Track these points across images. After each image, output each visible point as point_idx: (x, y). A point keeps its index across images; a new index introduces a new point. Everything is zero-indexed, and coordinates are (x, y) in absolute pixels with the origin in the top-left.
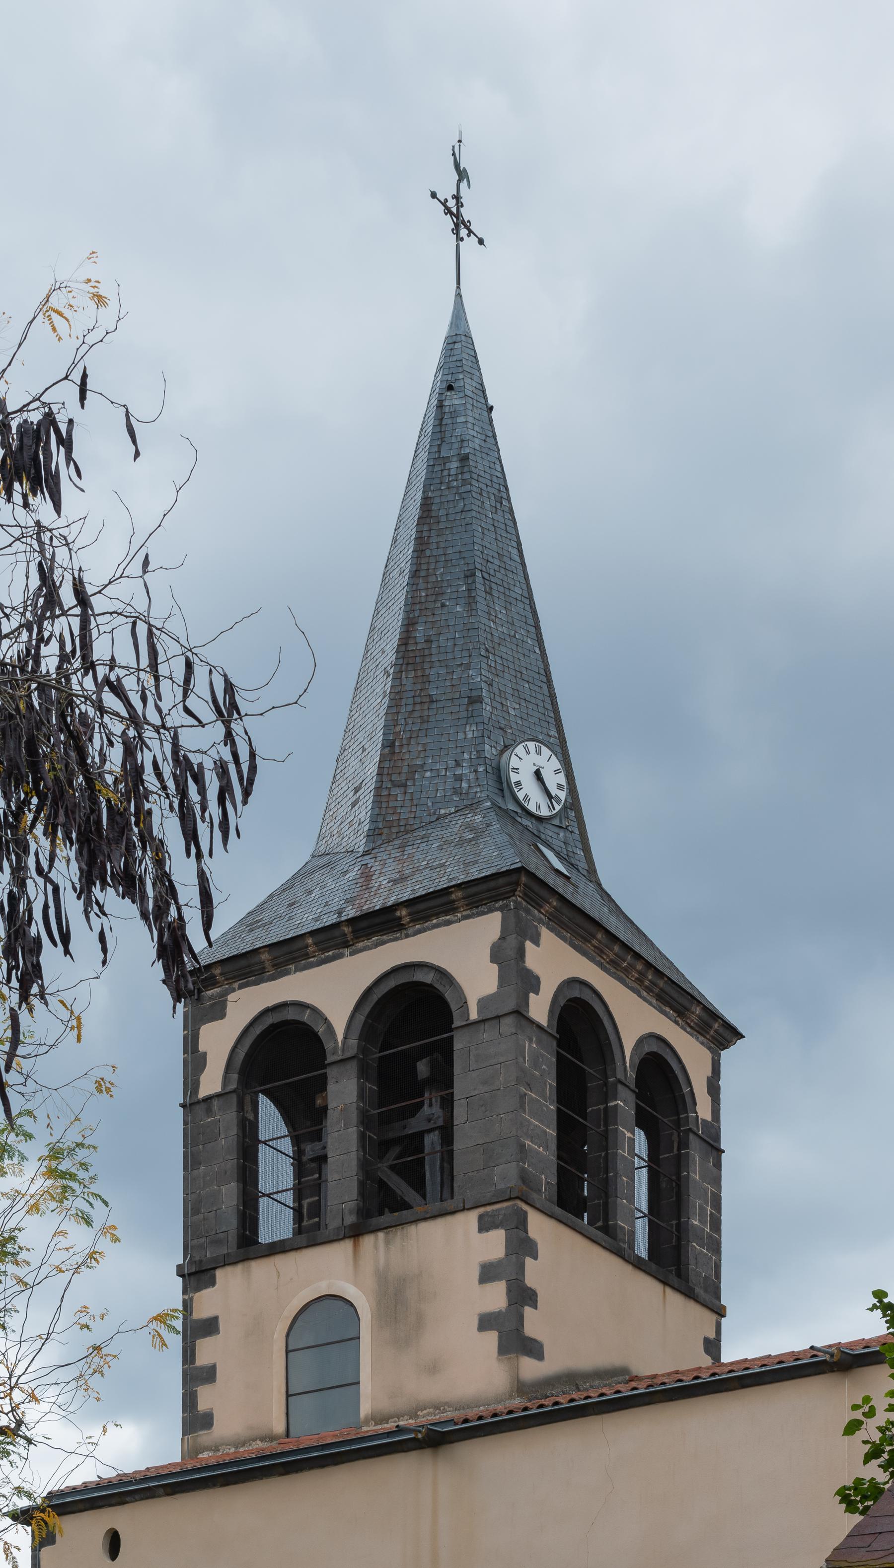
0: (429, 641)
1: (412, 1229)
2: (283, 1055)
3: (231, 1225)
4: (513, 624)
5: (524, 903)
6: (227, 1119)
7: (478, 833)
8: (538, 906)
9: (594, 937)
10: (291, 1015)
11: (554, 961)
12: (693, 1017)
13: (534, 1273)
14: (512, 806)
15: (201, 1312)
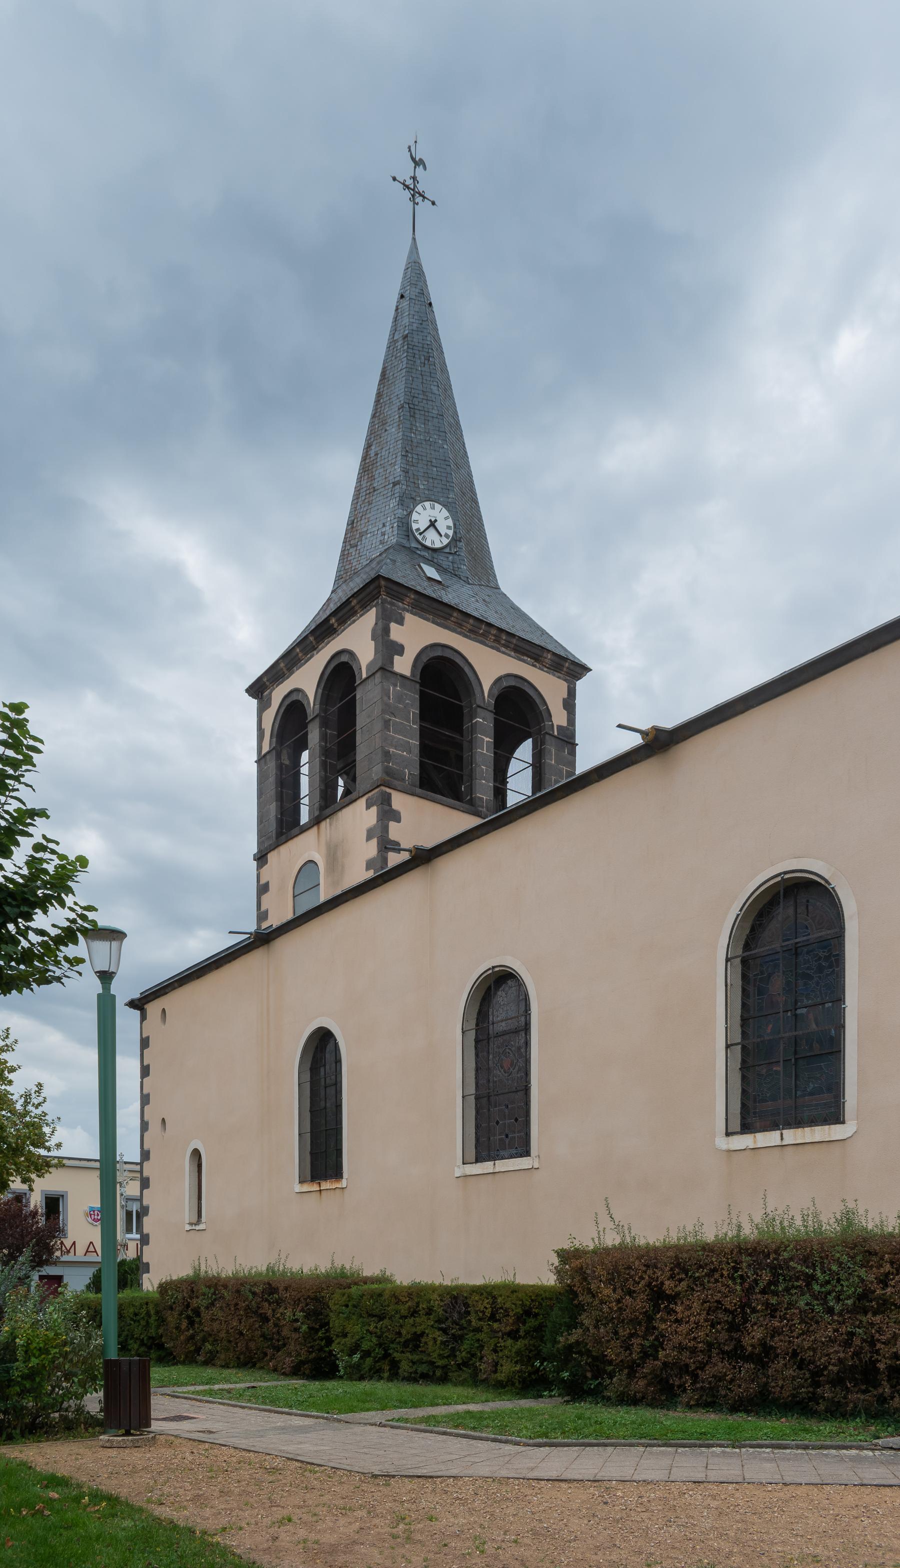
0: (377, 454)
1: (340, 814)
4: (428, 433)
5: (389, 599)
8: (402, 601)
9: (451, 616)
11: (416, 635)
12: (547, 661)
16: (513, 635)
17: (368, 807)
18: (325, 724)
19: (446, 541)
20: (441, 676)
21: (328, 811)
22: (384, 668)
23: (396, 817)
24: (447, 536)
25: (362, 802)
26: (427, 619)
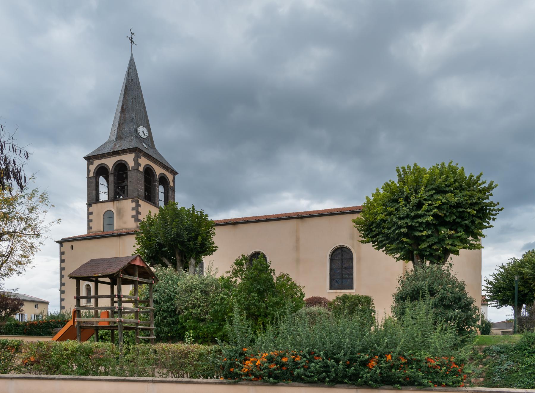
2: (102, 171)
3: (95, 197)
6: (94, 181)
7: (132, 140)
10: (103, 165)
11: (144, 162)
13: (140, 209)
15: (90, 211)
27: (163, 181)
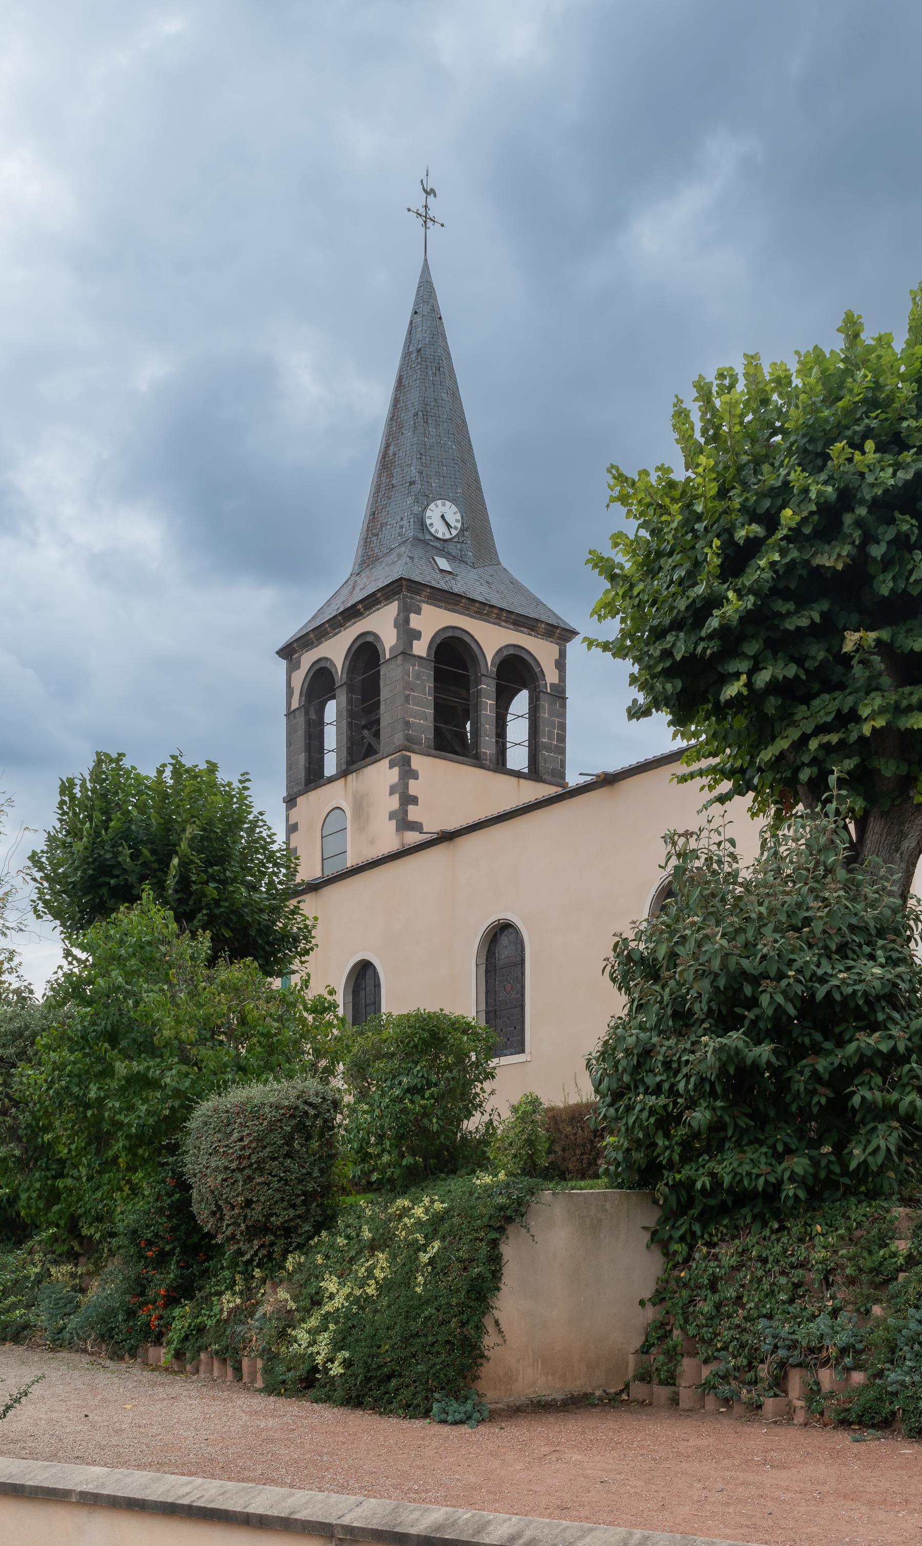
1: (365, 770)
8: (420, 595)
13: (414, 788)
14: (428, 537)
16: (512, 613)
17: (391, 767)
18: (351, 690)
19: (454, 532)
20: (453, 654)
21: (355, 767)
22: (405, 653)
23: (415, 775)
24: (456, 528)
25: (386, 762)
26: (440, 607)
27: (516, 671)
